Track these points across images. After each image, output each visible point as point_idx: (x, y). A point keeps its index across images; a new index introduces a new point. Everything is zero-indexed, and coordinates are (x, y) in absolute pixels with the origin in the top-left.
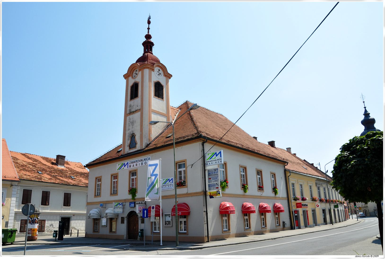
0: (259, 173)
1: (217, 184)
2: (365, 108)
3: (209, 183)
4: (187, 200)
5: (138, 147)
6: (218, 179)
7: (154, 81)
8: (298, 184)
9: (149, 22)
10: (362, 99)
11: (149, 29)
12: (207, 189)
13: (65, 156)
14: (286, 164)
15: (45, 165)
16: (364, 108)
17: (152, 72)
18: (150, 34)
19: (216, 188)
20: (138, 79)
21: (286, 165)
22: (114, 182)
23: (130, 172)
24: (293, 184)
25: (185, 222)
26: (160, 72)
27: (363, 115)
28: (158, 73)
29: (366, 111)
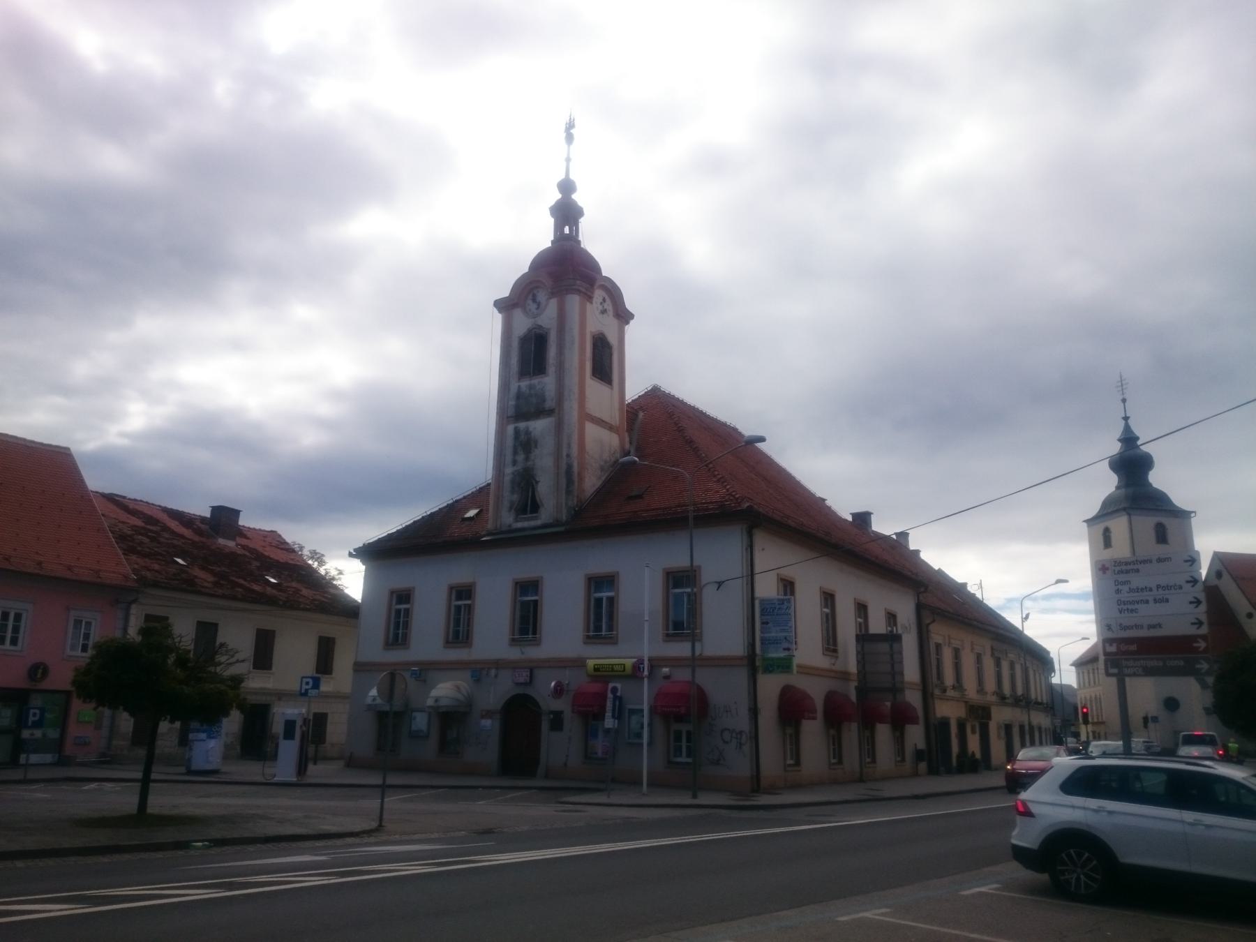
0: (829, 598)
1: (786, 638)
2: (1126, 419)
3: (762, 635)
4: (705, 678)
5: (545, 516)
6: (791, 627)
7: (591, 332)
8: (949, 646)
9: (570, 138)
10: (1121, 392)
11: (568, 160)
12: (758, 650)
13: (240, 511)
14: (922, 590)
15: (182, 537)
16: (1123, 418)
17: (588, 304)
18: (572, 177)
19: (785, 649)
20: (548, 317)
21: (920, 593)
22: (398, 611)
23: (517, 583)
24: (938, 646)
25: (689, 733)
26: (606, 306)
27: (1119, 440)
28: (600, 308)
29: (1127, 429)
